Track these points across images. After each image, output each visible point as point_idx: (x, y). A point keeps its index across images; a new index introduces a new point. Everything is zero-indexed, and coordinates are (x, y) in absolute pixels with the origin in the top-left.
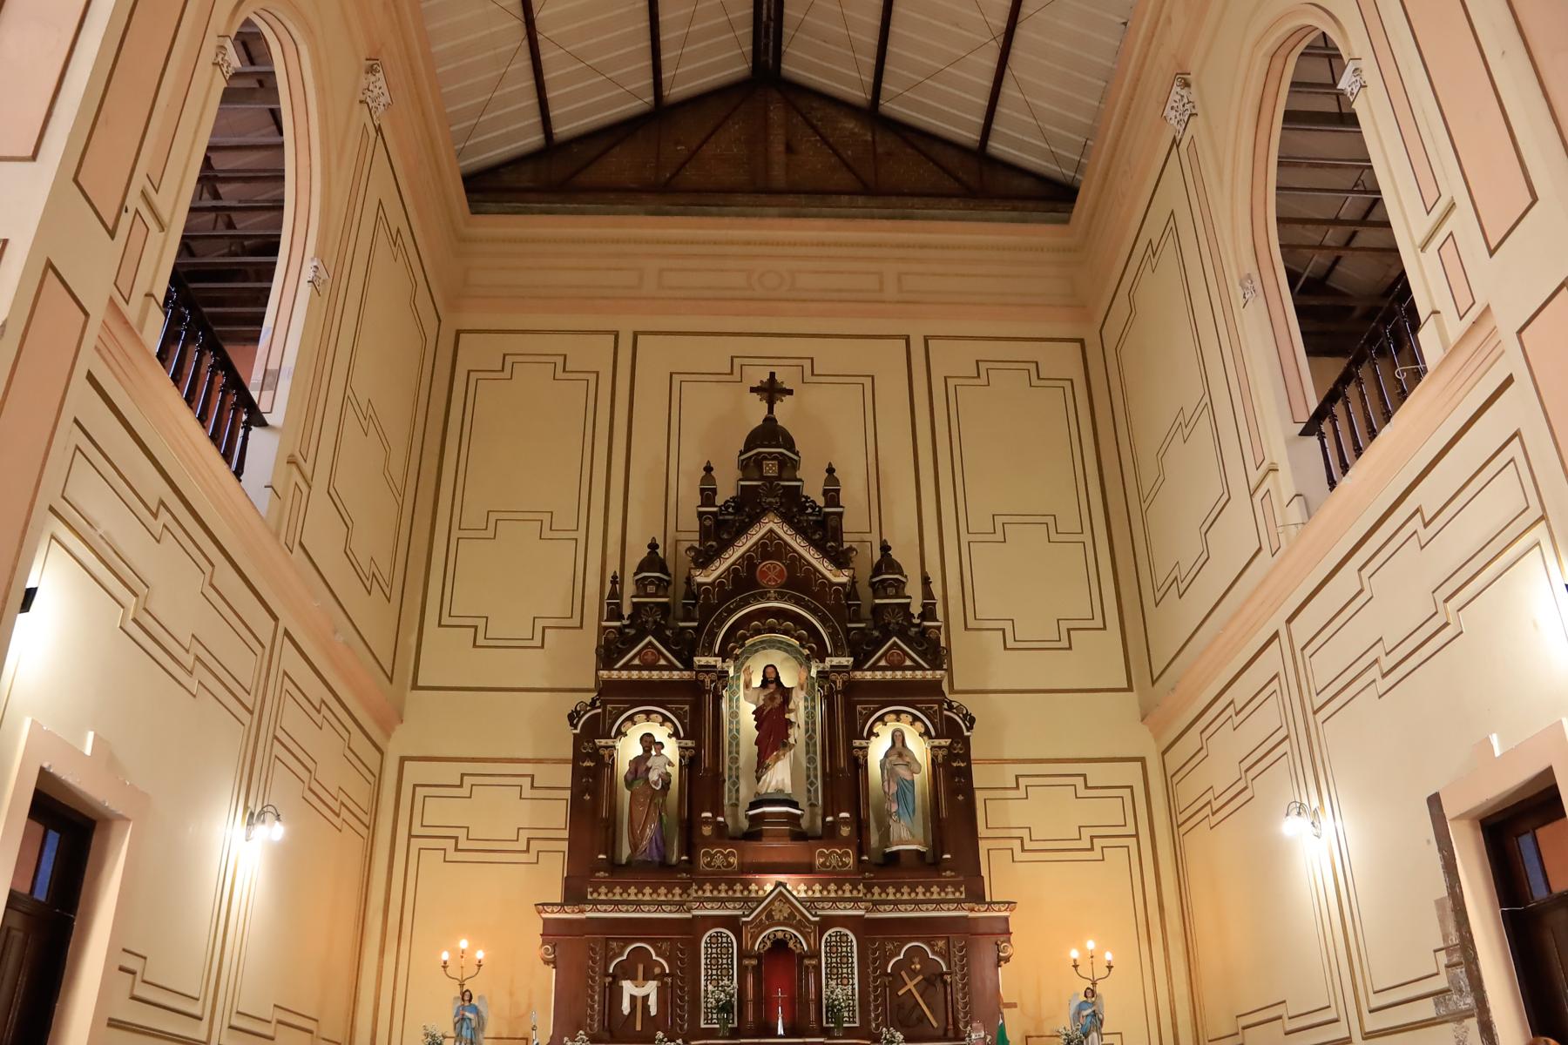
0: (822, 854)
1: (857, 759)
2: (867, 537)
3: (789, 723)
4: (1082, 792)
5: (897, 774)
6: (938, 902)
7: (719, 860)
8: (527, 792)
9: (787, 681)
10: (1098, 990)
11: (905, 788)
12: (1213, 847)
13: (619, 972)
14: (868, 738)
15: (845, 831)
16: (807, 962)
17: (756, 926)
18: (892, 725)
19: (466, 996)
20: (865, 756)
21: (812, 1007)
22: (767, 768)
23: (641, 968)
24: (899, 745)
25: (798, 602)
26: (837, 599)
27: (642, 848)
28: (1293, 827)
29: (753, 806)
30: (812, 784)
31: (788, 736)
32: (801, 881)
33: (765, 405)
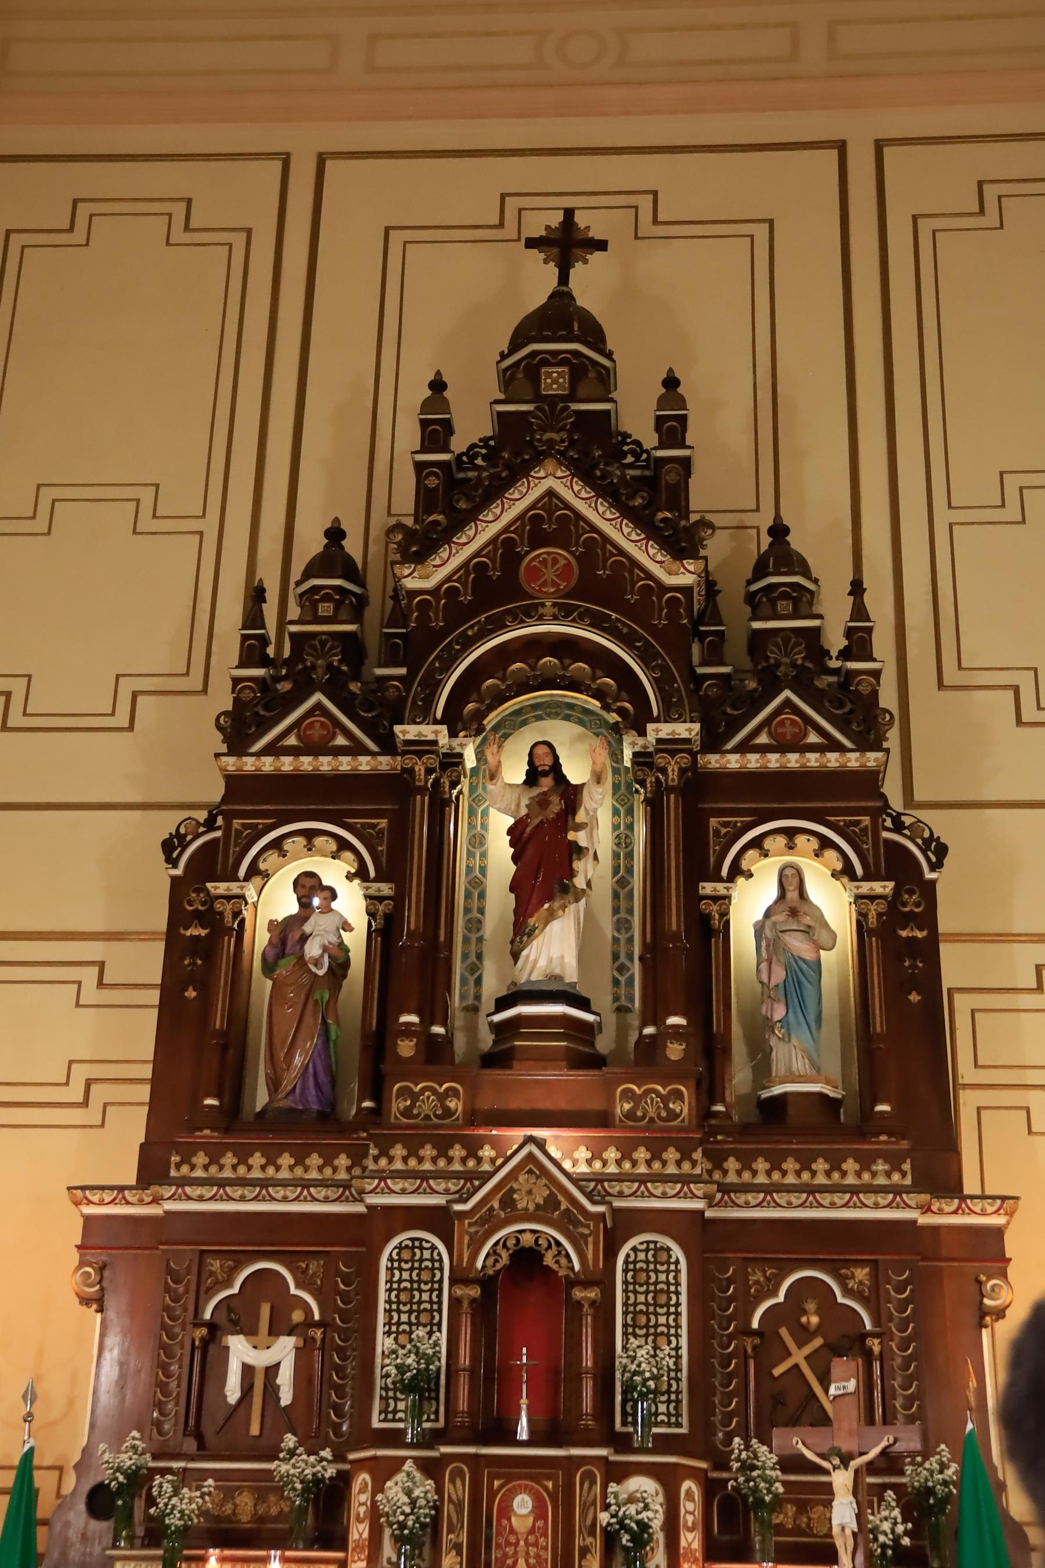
0: (627, 1095)
1: (707, 918)
2: (750, 519)
3: (577, 850)
5: (786, 949)
7: (428, 1105)
8: (91, 994)
9: (575, 772)
11: (801, 979)
13: (222, 1320)
15: (675, 1051)
16: (578, 1294)
20: (725, 914)
22: (531, 934)
23: (265, 1310)
24: (792, 895)
25: (598, 623)
26: (673, 616)
27: (286, 1085)
29: (502, 1004)
30: (622, 969)
31: (572, 874)
32: (578, 1142)
33: (552, 271)
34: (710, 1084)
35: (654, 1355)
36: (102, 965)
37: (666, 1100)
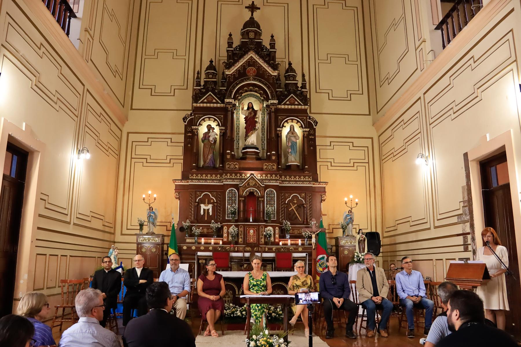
1: (278, 134)
2: (284, 60)
3: (256, 122)
4: (351, 148)
6: (303, 181)
7: (232, 166)
8: (170, 144)
9: (256, 108)
10: (353, 211)
11: (294, 144)
12: (393, 168)
14: (282, 127)
15: (274, 158)
16: (260, 199)
17: (244, 188)
18: (290, 124)
19: (151, 209)
20: (281, 134)
21: (261, 214)
23: (207, 200)
24: (292, 130)
25: (260, 81)
26: (273, 81)
28: (419, 162)
29: (244, 149)
30: (263, 142)
31: (255, 126)
33: (250, 13)
34: (279, 163)
35: (271, 208)
36: (171, 139)
37: (272, 166)
